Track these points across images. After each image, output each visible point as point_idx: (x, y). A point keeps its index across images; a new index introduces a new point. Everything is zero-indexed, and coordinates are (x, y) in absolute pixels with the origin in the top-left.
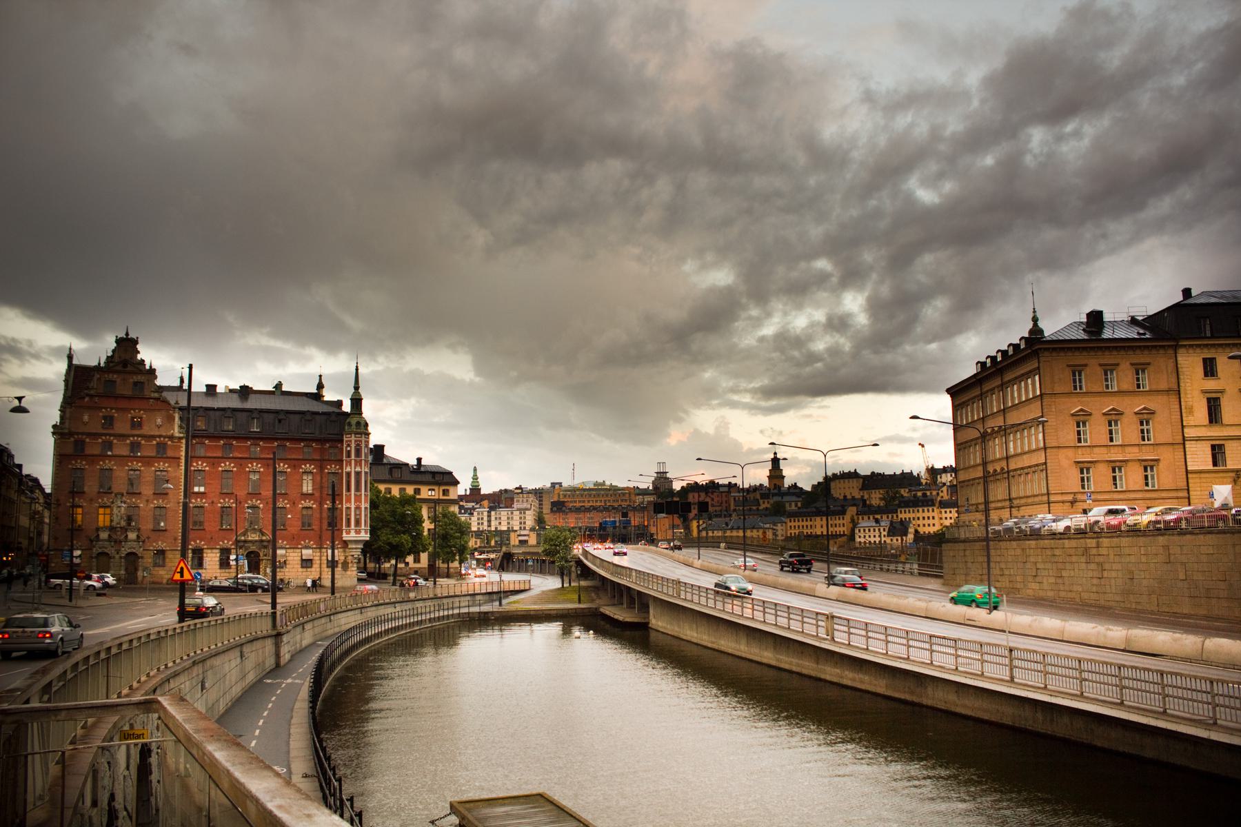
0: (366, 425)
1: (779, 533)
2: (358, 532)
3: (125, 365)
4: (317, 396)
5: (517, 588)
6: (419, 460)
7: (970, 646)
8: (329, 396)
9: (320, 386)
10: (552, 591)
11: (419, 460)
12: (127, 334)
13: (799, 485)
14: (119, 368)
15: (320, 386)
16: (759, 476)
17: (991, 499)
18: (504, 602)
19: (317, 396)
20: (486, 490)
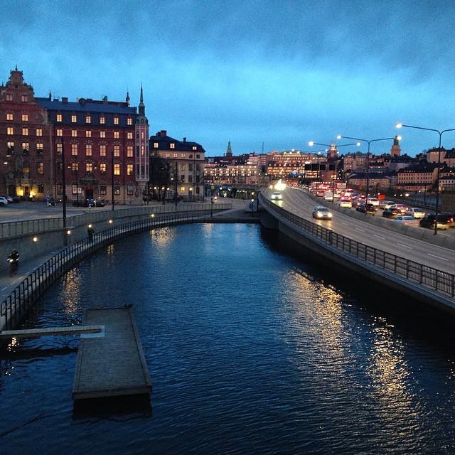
0: (147, 121)
1: (393, 182)
2: (143, 177)
3: (16, 87)
4: (126, 105)
5: (224, 208)
6: (185, 139)
7: (415, 266)
8: (131, 105)
9: (128, 99)
10: (238, 211)
11: (185, 139)
12: (16, 69)
13: (408, 154)
14: (14, 87)
15: (128, 99)
16: (387, 149)
17: (437, 147)
18: (213, 215)
19: (126, 105)
20: (235, 154)
